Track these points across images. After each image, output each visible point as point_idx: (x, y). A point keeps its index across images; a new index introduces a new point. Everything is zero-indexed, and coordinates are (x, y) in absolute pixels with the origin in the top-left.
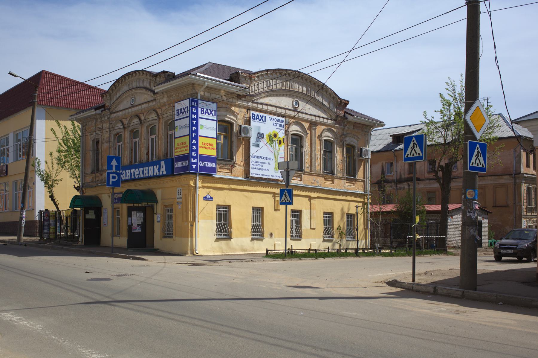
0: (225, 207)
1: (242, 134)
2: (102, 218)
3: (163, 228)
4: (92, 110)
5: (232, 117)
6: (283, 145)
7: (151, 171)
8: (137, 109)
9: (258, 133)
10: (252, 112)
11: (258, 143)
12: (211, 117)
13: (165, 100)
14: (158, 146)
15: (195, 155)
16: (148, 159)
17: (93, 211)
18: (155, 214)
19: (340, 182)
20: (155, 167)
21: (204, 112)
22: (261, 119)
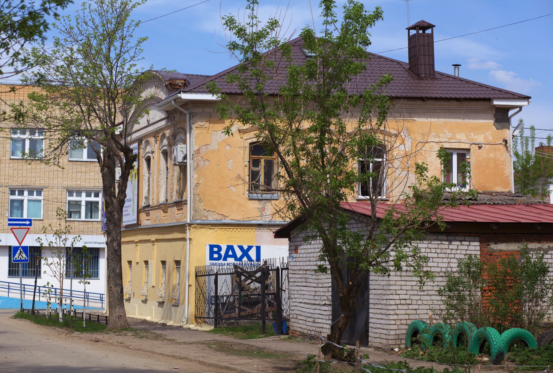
21: (220, 256)
22: (242, 257)
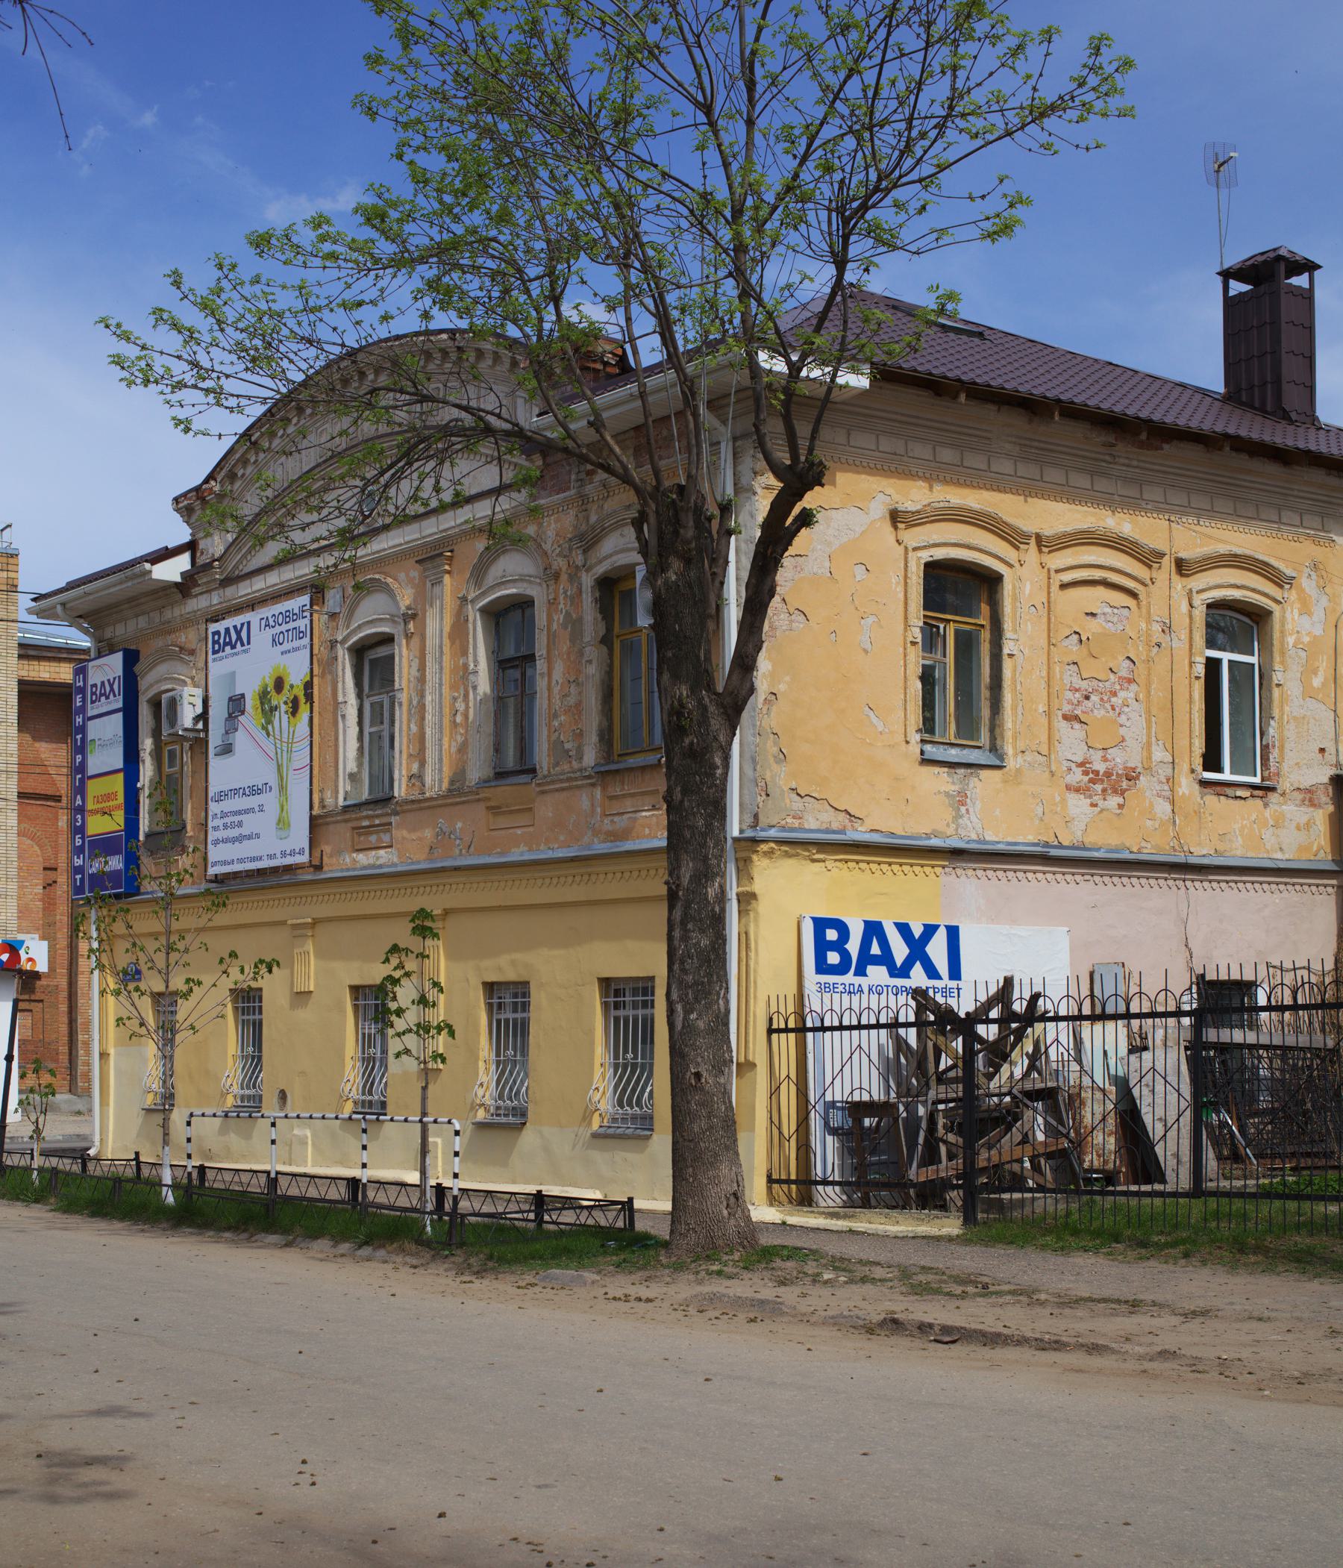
21: (845, 956)
22: (908, 964)
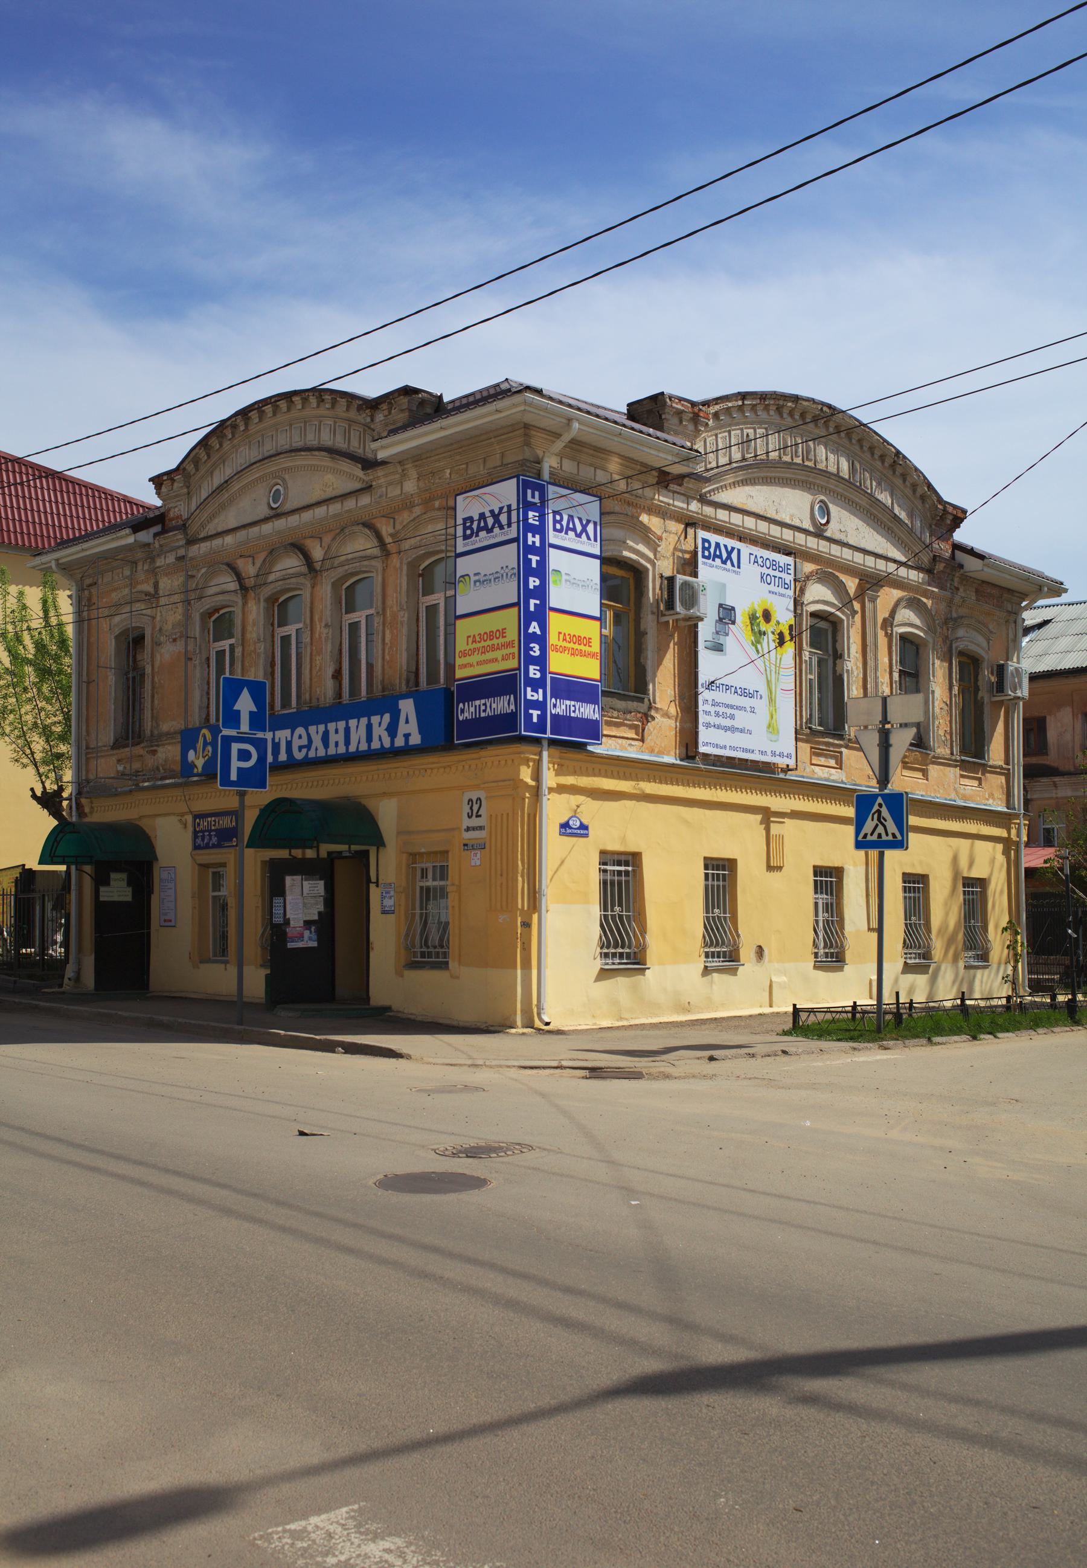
0: (623, 858)
1: (679, 608)
2: (155, 899)
3: (407, 935)
4: (123, 533)
5: (641, 547)
6: (789, 648)
7: (358, 734)
8: (295, 525)
9: (721, 606)
10: (702, 534)
11: (721, 640)
12: (583, 543)
13: (410, 486)
14: (383, 650)
15: (538, 675)
16: (339, 695)
17: (124, 876)
18: (372, 887)
19: (944, 774)
20: (375, 719)
